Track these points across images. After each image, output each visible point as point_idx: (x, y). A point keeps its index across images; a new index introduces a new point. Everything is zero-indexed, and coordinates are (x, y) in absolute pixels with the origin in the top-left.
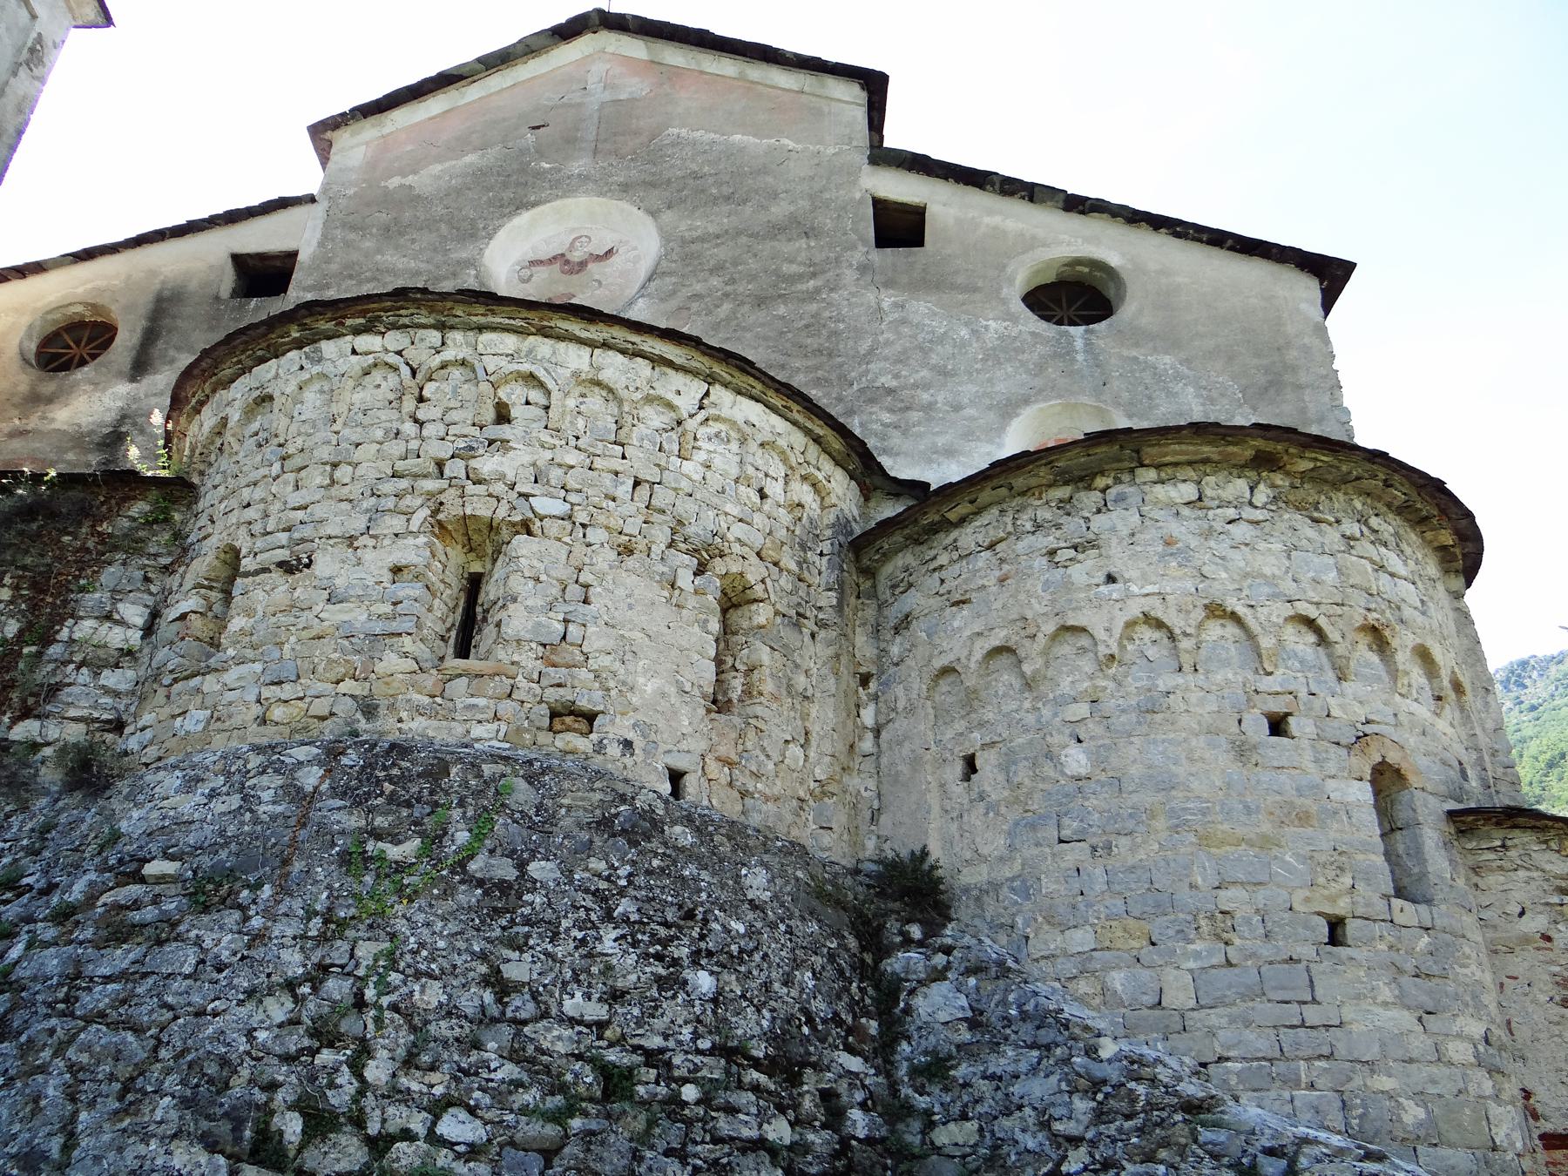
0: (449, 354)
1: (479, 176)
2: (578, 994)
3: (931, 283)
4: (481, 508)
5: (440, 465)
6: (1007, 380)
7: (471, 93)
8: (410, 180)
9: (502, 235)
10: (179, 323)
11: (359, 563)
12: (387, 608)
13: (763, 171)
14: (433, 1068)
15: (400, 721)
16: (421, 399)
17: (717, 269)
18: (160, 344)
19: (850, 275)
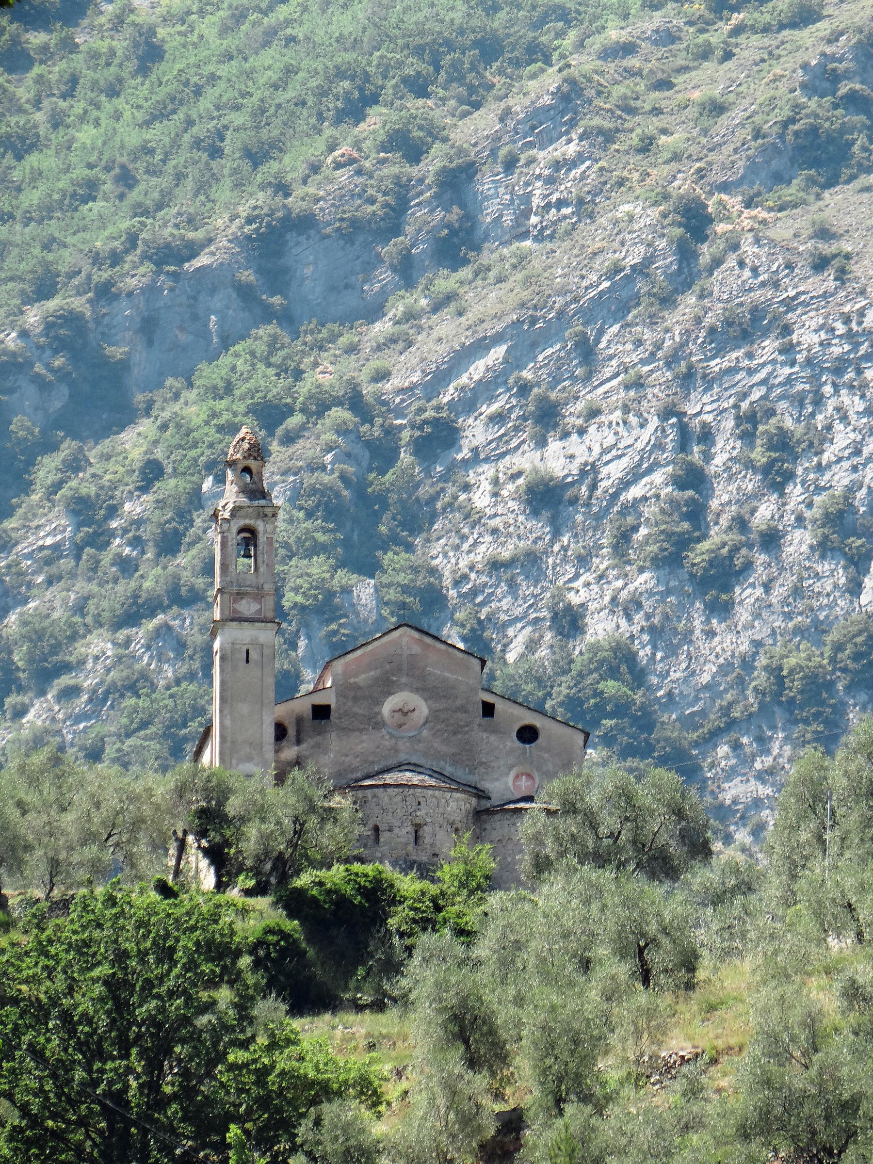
1: (376, 679)
3: (495, 731)
4: (418, 822)
6: (511, 760)
13: (453, 688)
17: (443, 721)
19: (476, 727)
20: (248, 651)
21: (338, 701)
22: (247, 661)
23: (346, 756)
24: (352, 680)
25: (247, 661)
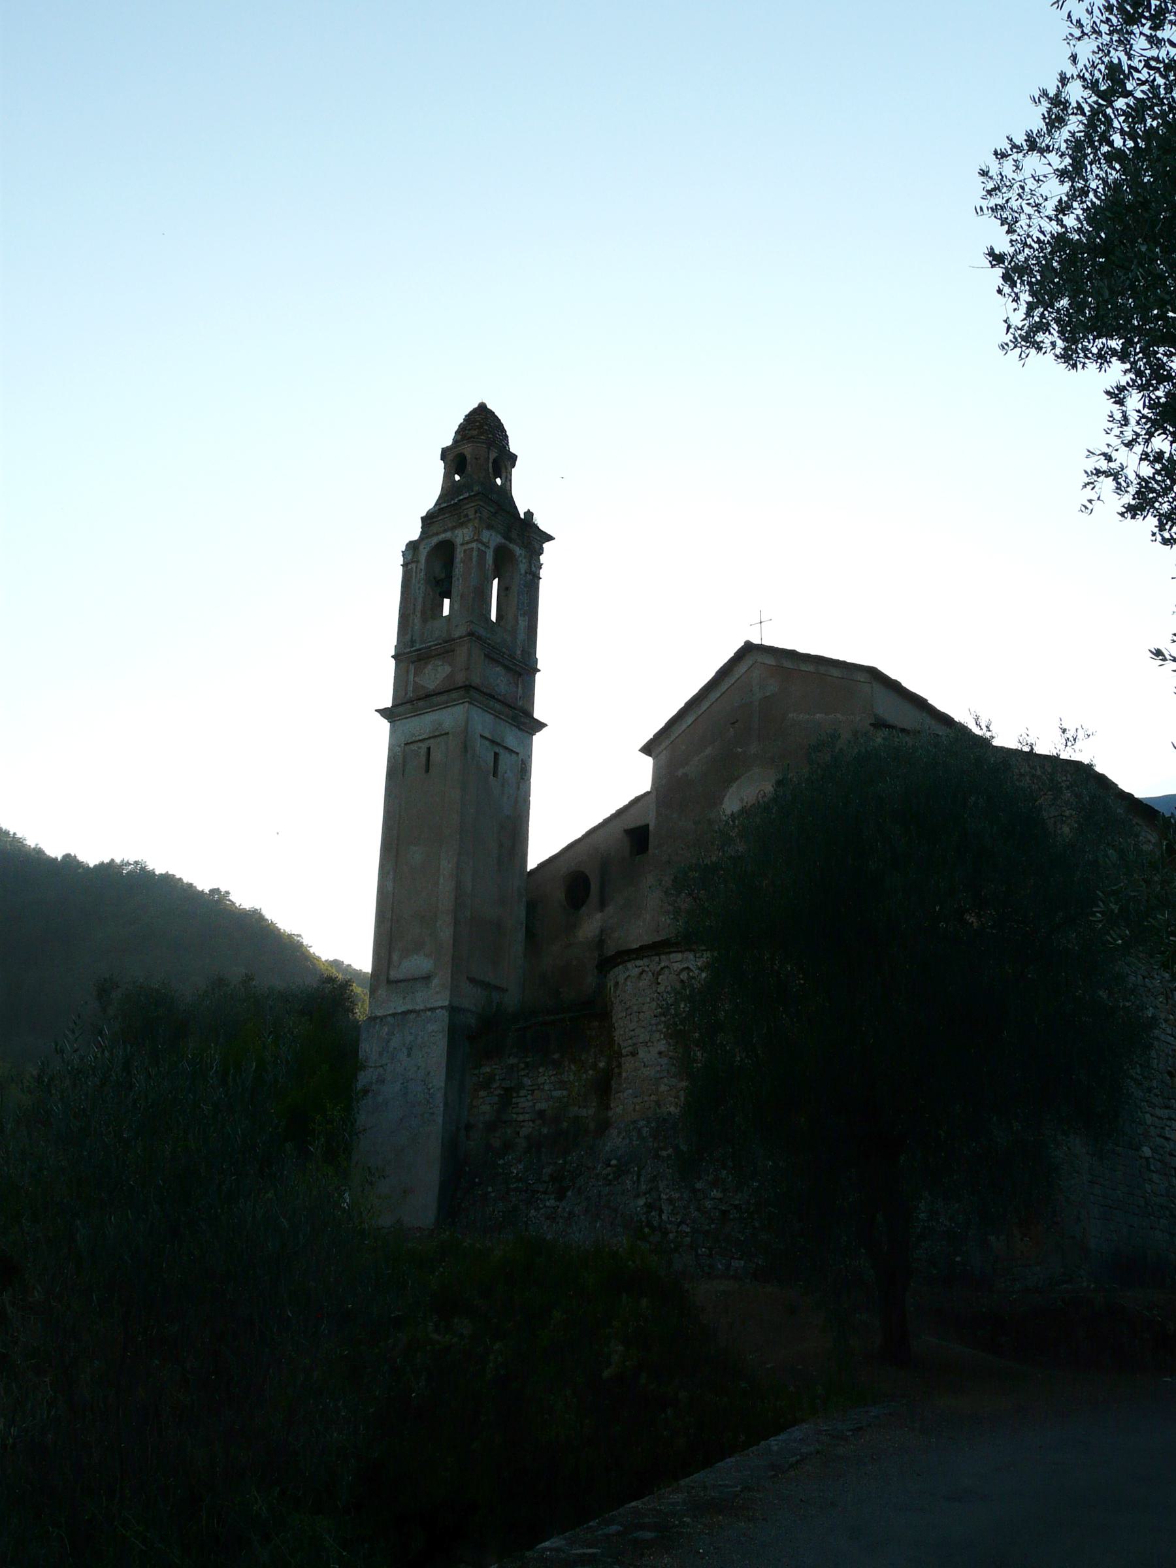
0: (662, 965)
2: (715, 1191)
7: (705, 706)
9: (726, 799)
11: (649, 1052)
12: (658, 1068)
14: (677, 1214)
15: (667, 1108)
16: (659, 984)
20: (429, 749)
22: (427, 770)
24: (680, 773)
25: (427, 770)
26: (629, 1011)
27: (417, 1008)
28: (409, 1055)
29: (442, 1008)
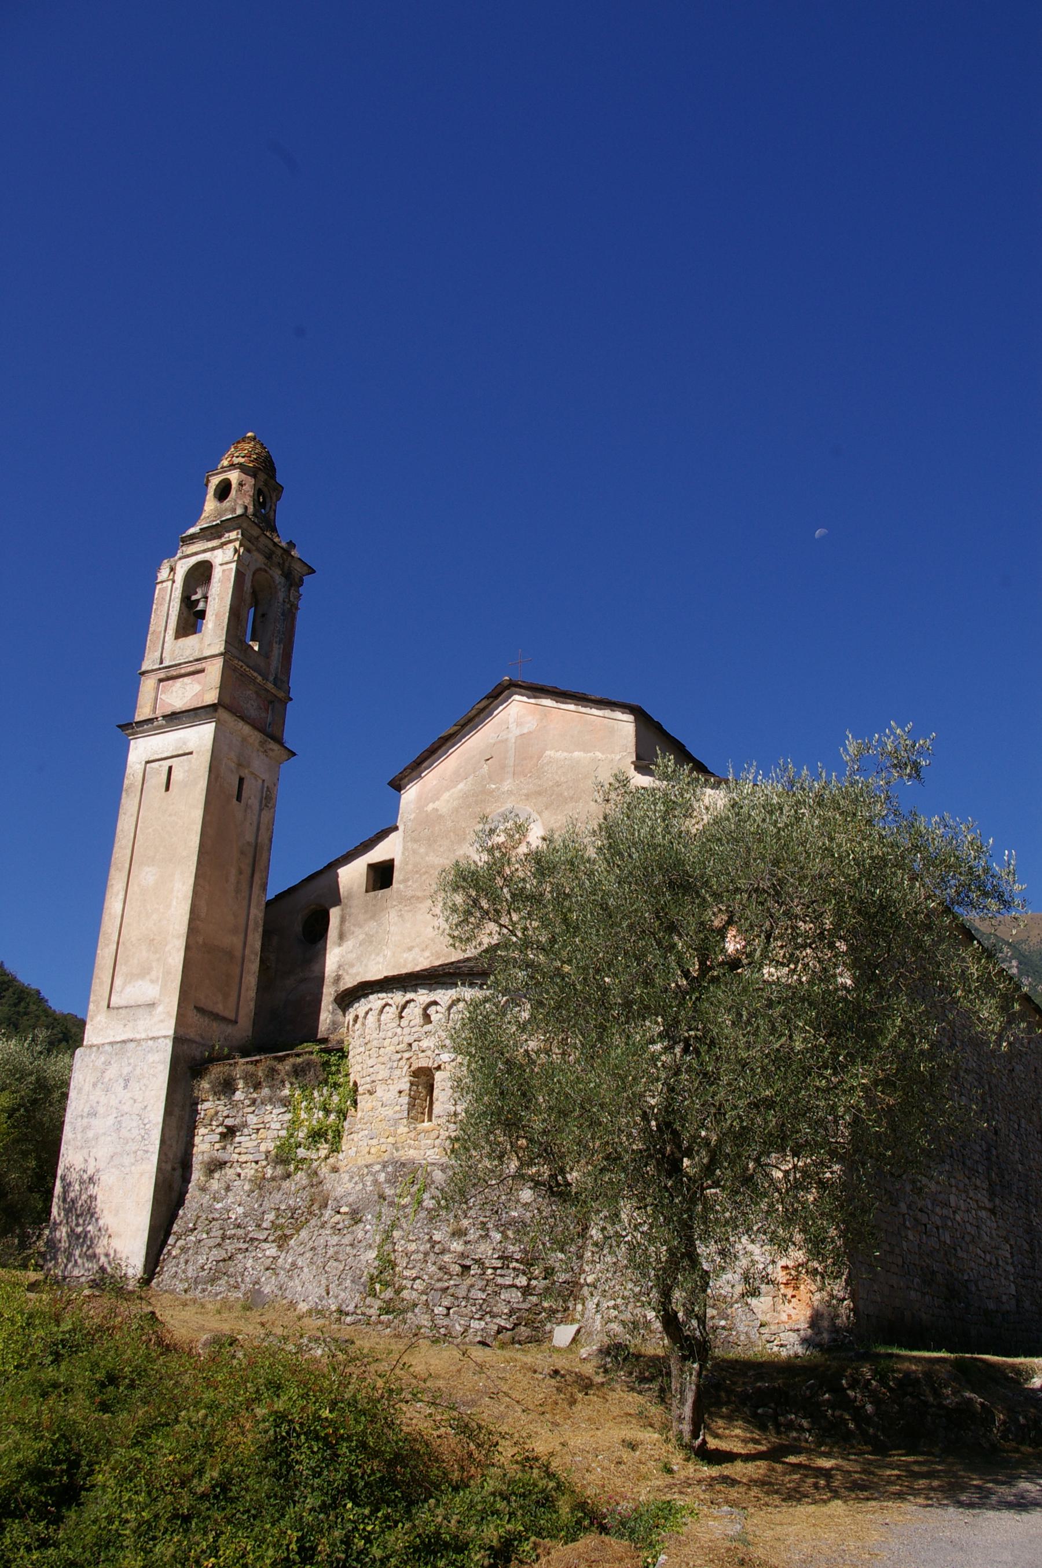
5: (410, 1045)
8: (436, 805)
10: (353, 910)
18: (347, 924)
21: (405, 849)
22: (167, 789)
23: (410, 949)
24: (430, 807)
25: (167, 789)
26: (369, 1046)
27: (138, 1036)
28: (125, 1087)
29: (165, 1037)
